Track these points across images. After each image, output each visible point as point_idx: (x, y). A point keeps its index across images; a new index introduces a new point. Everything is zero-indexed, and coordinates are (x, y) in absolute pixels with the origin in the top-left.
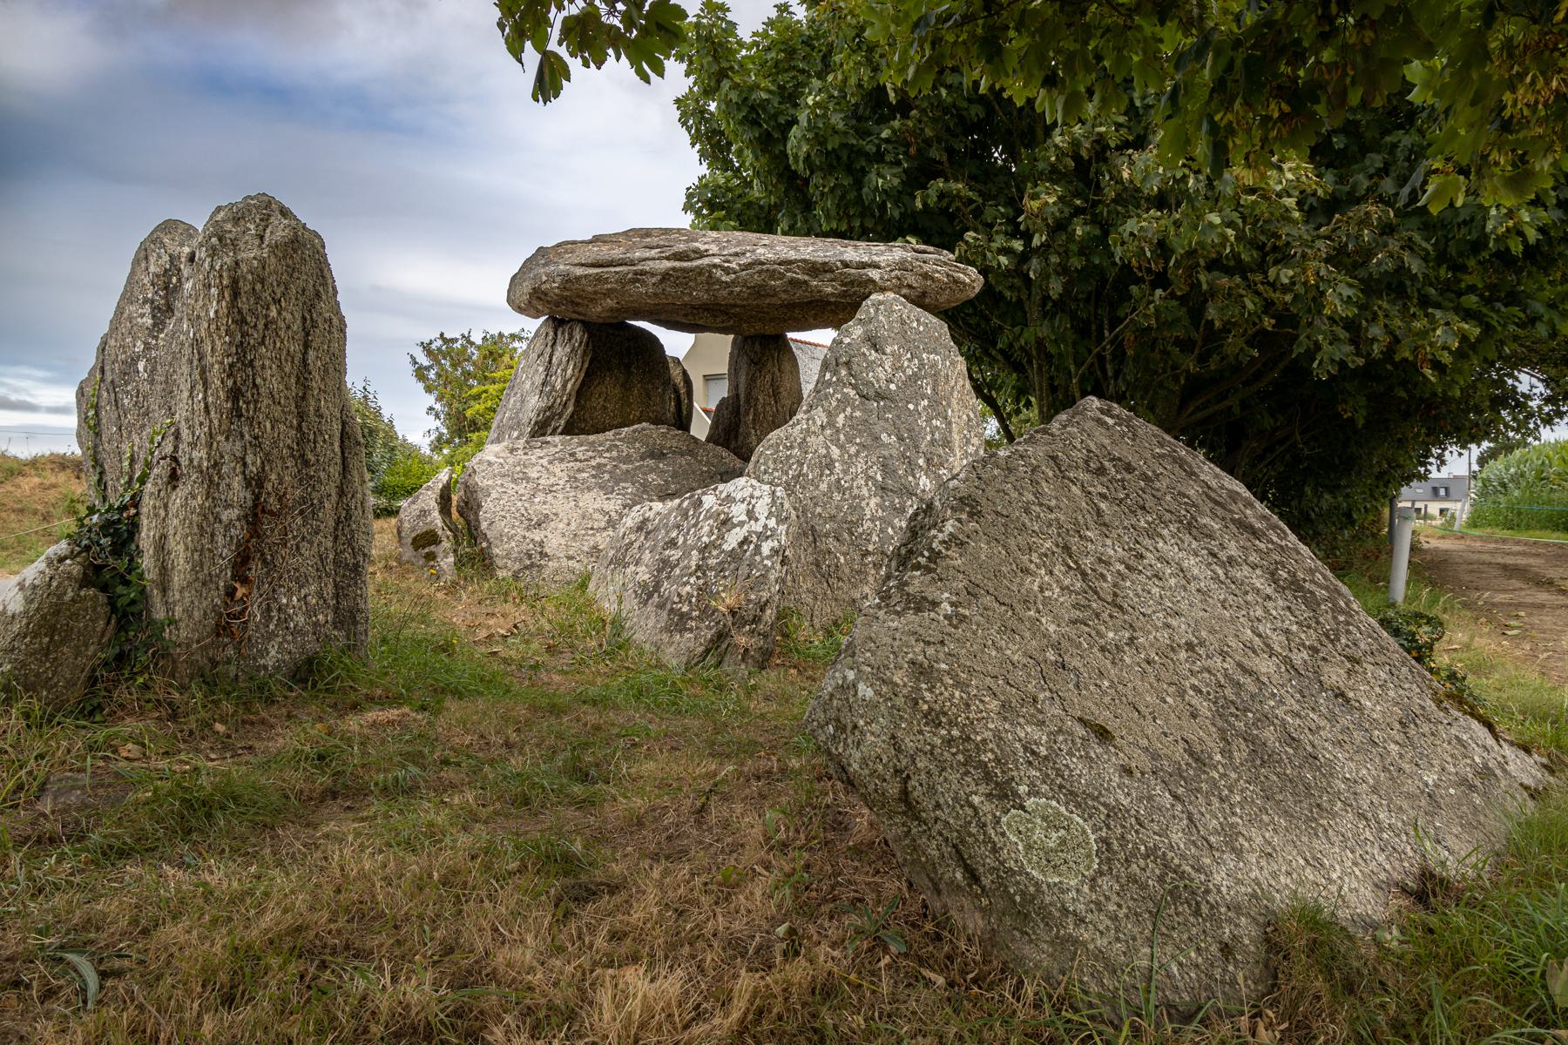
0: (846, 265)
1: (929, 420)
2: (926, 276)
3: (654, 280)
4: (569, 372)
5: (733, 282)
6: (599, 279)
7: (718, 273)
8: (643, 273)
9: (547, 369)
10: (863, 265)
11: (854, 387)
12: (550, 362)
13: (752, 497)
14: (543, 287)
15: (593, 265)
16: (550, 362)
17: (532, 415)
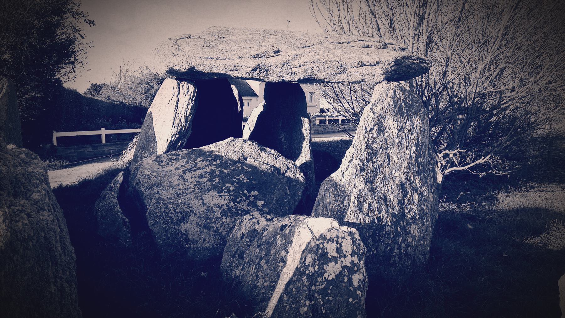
4: (189, 111)
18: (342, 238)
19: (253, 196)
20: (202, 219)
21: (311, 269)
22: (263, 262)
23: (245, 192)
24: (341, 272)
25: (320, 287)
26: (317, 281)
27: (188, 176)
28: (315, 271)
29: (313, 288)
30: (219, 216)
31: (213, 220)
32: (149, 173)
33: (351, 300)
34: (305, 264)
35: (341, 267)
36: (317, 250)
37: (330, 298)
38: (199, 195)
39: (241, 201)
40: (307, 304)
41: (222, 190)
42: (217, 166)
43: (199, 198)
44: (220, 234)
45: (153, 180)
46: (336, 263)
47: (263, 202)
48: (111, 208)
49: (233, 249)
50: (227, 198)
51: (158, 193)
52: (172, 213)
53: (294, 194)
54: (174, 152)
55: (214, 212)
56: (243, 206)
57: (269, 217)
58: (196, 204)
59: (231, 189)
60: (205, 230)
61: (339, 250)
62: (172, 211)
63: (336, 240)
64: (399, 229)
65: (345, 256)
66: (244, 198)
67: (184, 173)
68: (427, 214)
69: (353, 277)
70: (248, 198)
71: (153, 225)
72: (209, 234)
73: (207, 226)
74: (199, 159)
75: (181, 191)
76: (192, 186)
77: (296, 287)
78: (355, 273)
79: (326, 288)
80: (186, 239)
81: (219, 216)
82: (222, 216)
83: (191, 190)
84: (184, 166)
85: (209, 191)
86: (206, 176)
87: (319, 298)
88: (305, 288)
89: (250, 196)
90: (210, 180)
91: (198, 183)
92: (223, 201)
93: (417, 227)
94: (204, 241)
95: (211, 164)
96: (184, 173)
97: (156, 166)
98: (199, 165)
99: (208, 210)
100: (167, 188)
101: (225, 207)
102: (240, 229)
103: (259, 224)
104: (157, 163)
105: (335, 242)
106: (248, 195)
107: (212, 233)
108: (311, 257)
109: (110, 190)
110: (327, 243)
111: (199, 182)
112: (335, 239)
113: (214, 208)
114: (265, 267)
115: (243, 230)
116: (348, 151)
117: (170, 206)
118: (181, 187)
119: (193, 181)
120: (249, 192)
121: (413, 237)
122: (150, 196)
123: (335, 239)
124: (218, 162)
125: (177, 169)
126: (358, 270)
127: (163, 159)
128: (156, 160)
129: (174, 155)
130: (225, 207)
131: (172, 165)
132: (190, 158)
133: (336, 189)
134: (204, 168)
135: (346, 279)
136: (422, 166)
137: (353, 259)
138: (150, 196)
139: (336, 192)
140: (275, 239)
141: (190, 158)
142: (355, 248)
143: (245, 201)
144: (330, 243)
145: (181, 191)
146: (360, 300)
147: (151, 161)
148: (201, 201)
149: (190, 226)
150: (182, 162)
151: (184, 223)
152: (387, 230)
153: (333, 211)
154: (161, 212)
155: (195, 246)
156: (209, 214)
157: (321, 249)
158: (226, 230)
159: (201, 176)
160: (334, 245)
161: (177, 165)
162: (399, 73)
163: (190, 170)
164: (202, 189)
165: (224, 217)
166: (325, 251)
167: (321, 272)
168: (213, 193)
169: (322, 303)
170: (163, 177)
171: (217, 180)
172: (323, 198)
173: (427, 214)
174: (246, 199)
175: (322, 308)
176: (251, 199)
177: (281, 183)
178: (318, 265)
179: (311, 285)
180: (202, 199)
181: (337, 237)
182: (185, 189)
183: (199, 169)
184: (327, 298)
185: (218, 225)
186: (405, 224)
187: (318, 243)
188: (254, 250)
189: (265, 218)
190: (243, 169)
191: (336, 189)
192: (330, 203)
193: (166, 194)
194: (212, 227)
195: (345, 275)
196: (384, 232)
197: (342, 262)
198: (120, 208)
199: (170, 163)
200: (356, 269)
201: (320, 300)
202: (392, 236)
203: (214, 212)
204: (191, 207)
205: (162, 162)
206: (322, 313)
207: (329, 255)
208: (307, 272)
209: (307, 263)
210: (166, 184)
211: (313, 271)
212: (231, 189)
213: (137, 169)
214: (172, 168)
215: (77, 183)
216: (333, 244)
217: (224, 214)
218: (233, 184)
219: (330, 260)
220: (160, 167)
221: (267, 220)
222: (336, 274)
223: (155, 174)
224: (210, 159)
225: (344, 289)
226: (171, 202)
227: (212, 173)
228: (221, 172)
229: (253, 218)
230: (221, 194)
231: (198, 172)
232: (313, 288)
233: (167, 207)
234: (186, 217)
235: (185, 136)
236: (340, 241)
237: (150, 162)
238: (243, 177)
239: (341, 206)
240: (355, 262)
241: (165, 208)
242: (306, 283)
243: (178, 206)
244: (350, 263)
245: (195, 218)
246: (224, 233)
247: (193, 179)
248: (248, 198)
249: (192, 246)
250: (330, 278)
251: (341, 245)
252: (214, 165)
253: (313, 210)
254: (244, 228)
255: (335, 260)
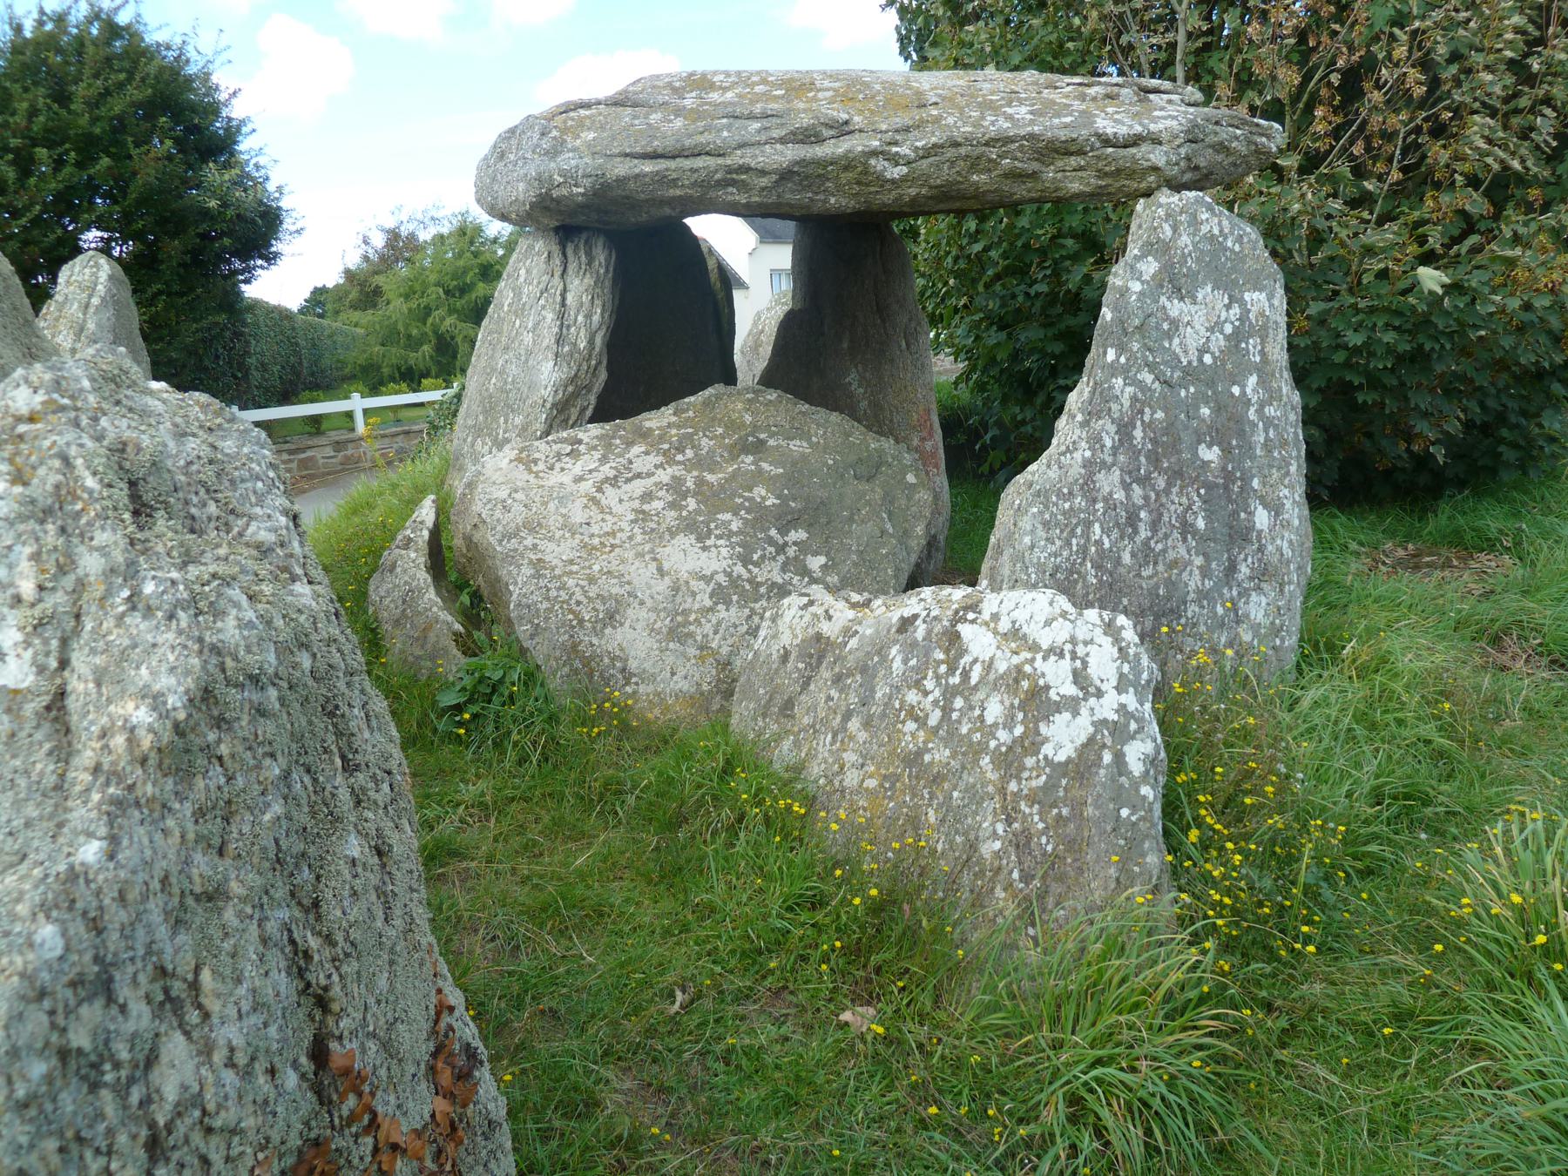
0: (1107, 141)
1: (1260, 411)
2: (1221, 148)
3: (764, 181)
4: (596, 318)
5: (904, 179)
6: (661, 179)
7: (878, 164)
8: (745, 169)
9: (561, 316)
10: (1135, 141)
11: (1152, 367)
12: (563, 304)
13: (1073, 641)
14: (555, 193)
15: (654, 156)
16: (563, 304)
17: (547, 393)
18: (1086, 643)
19: (795, 543)
20: (662, 615)
21: (1003, 735)
22: (854, 725)
23: (773, 532)
24: (1091, 740)
25: (1034, 783)
26: (1022, 768)
27: (611, 496)
28: (1014, 741)
29: (1013, 786)
30: (708, 603)
31: (692, 617)
32: (503, 494)
33: (1125, 812)
34: (983, 721)
35: (1093, 723)
36: (1017, 681)
37: (1065, 811)
38: (647, 547)
39: (763, 557)
40: (1000, 831)
41: (710, 532)
42: (688, 466)
43: (647, 557)
44: (715, 653)
45: (518, 514)
46: (1076, 713)
47: (822, 560)
48: (409, 597)
49: (762, 691)
50: (724, 551)
51: (535, 546)
52: (578, 603)
53: (905, 532)
54: (565, 434)
55: (694, 594)
56: (771, 572)
57: (855, 597)
58: (641, 574)
59: (734, 527)
60: (671, 645)
61: (1080, 677)
62: (579, 596)
63: (1068, 651)
64: (1220, 610)
65: (1099, 694)
66: (772, 549)
67: (600, 490)
68: (1289, 562)
69: (1126, 749)
70: (781, 549)
71: (532, 637)
72: (684, 655)
73: (677, 634)
74: (637, 449)
75: (596, 541)
76: (625, 525)
77: (962, 785)
78: (1133, 738)
79: (1049, 787)
80: (623, 670)
81: (708, 603)
82: (716, 604)
83: (624, 536)
84: (596, 470)
85: (673, 535)
86: (660, 494)
87: (1031, 814)
88: (990, 789)
89: (786, 544)
90: (672, 505)
91: (642, 516)
92: (717, 560)
93: (1264, 601)
94: (673, 674)
95: (671, 461)
96: (600, 490)
97: (521, 475)
98: (638, 466)
99: (676, 589)
100: (558, 534)
101: (721, 578)
102: (775, 636)
103: (830, 618)
104: (522, 467)
105: (1068, 656)
106: (781, 542)
107: (692, 651)
108: (1002, 702)
109: (406, 547)
110: (1045, 659)
111: (643, 512)
112: (1068, 647)
113: (692, 583)
114: (862, 736)
115: (786, 639)
116: (1072, 397)
117: (571, 582)
118: (595, 529)
119: (625, 511)
120: (783, 531)
121: (1256, 628)
122: (512, 558)
123: (1068, 647)
124: (689, 453)
125: (579, 479)
126: (1140, 730)
127: (537, 455)
128: (519, 460)
129: (562, 441)
130: (721, 578)
131: (563, 470)
132: (609, 447)
133: (1047, 507)
134: (653, 474)
135: (1107, 757)
136: (1276, 427)
137: (1124, 698)
138: (512, 558)
139: (1047, 516)
140: (884, 659)
141: (609, 447)
142: (1126, 668)
143: (774, 558)
144: (1053, 658)
145: (596, 541)
146: (1151, 810)
147: (507, 460)
148: (653, 566)
149: (630, 634)
150: (589, 461)
151: (614, 628)
152: (1190, 614)
153: (1041, 568)
154: (548, 599)
155: (650, 689)
156: (679, 599)
157: (1028, 677)
158: (730, 641)
159: (647, 497)
160: (1066, 664)
161: (577, 469)
162: (1197, 168)
163: (613, 482)
164: (653, 530)
165: (720, 607)
166: (1041, 682)
167: (1031, 743)
168: (685, 541)
169: (1041, 826)
170: (545, 504)
171: (692, 503)
172: (1010, 536)
173: (1289, 562)
174: (778, 553)
175: (1044, 840)
176: (791, 551)
177: (868, 503)
178: (1022, 722)
179: (1005, 780)
180: (655, 559)
181: (1073, 641)
182: (608, 534)
183: (639, 476)
184: (1055, 811)
185: (708, 628)
186: (1235, 593)
187: (1016, 660)
188: (822, 691)
189: (847, 601)
190: (760, 471)
191: (1047, 507)
192: (1032, 547)
193: (558, 552)
194: (691, 635)
195: (1104, 746)
196: (1183, 621)
197: (1092, 709)
198: (438, 593)
199: (558, 466)
200: (1133, 726)
201: (1036, 818)
202: (1202, 628)
203: (694, 594)
204: (629, 583)
205: (535, 462)
206: (1045, 854)
207: (1053, 695)
208: (993, 744)
209: (989, 720)
210: (554, 521)
211: (1009, 742)
212: (734, 527)
213: (471, 485)
214: (566, 479)
215: (786, 285)
216: (1062, 662)
217: (720, 596)
218: (736, 514)
219: (1057, 708)
220: (531, 478)
221: (854, 606)
222: (1079, 742)
223: (520, 496)
224: (666, 446)
225: (1104, 785)
226: (571, 573)
227: (676, 486)
228: (700, 482)
229: (811, 603)
230: (708, 543)
231: (638, 487)
232: (1013, 786)
233: (563, 587)
234: (616, 611)
235: (588, 388)
236: (1081, 650)
237: (504, 463)
238: (763, 492)
239: (1065, 553)
240: (1131, 708)
241: (559, 589)
242: (992, 776)
243: (592, 580)
244: (1117, 711)
245: (643, 614)
246: (725, 650)
247: (626, 505)
248: (781, 549)
249: (642, 688)
250: (1061, 757)
251: (1085, 664)
252: (679, 463)
253: (985, 567)
254: (788, 632)
255: (1072, 705)
